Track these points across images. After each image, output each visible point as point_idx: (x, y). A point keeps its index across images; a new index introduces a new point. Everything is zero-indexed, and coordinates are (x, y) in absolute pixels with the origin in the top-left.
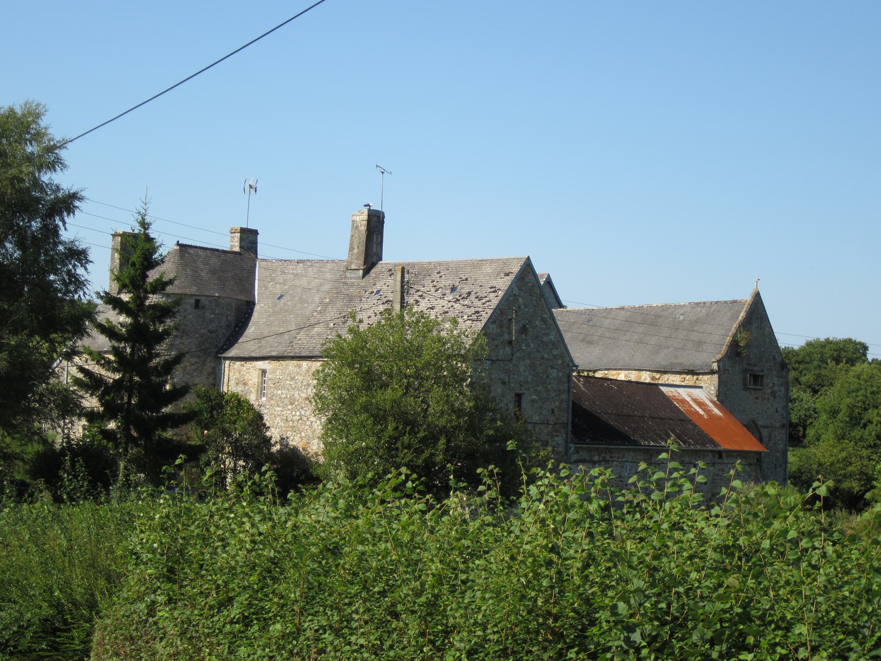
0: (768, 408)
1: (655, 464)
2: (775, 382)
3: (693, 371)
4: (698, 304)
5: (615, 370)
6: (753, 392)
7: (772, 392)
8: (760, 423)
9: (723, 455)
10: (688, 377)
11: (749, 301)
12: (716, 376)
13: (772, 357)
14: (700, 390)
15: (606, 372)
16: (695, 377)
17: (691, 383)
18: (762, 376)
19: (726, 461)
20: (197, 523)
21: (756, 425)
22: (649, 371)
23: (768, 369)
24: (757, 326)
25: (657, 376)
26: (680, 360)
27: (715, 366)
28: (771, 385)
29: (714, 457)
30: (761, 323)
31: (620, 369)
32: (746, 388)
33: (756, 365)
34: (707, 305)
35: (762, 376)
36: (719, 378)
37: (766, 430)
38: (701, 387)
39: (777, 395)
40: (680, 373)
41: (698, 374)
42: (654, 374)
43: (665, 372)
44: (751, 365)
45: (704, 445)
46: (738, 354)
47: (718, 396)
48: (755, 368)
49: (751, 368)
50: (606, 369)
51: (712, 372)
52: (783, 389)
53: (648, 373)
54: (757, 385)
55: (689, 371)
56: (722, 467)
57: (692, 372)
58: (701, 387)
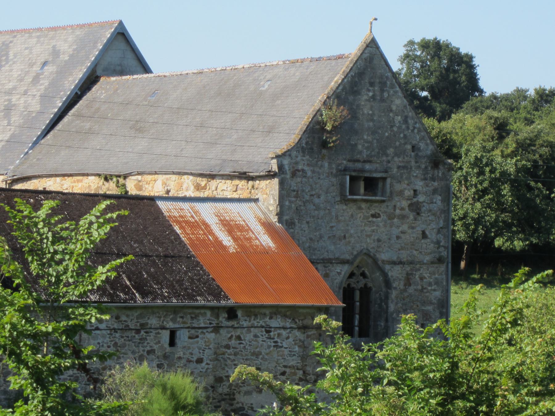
0: (403, 232)
1: (244, 328)
2: (417, 188)
3: (245, 173)
4: (293, 62)
5: (150, 174)
6: (363, 205)
7: (410, 205)
8: (383, 256)
9: (239, 313)
10: (242, 183)
11: (352, 56)
12: (276, 181)
13: (409, 147)
14: (253, 204)
15: (139, 177)
16: (251, 183)
17: (245, 195)
18: (384, 179)
19: (245, 324)
20: (526, 384)
21: (375, 261)
22: (191, 174)
23: (399, 167)
24: (373, 97)
25: (203, 182)
26: (237, 157)
27: (274, 166)
28: (408, 193)
29: (217, 317)
30: (382, 91)
31: (156, 173)
32: (344, 200)
33: (370, 162)
34: (299, 61)
35: (384, 179)
36: (281, 183)
37: (398, 268)
38: (256, 200)
39: (423, 209)
40: (230, 177)
41: (253, 179)
42: (199, 179)
43: (212, 177)
44: (358, 161)
45: (191, 297)
46: (324, 144)
47: (280, 215)
48: (367, 166)
49: (359, 165)
50: (139, 174)
51: (270, 175)
52: (438, 199)
53: (191, 177)
54: (375, 195)
55: (241, 173)
56: (238, 332)
57: (244, 176)
58: (256, 200)
